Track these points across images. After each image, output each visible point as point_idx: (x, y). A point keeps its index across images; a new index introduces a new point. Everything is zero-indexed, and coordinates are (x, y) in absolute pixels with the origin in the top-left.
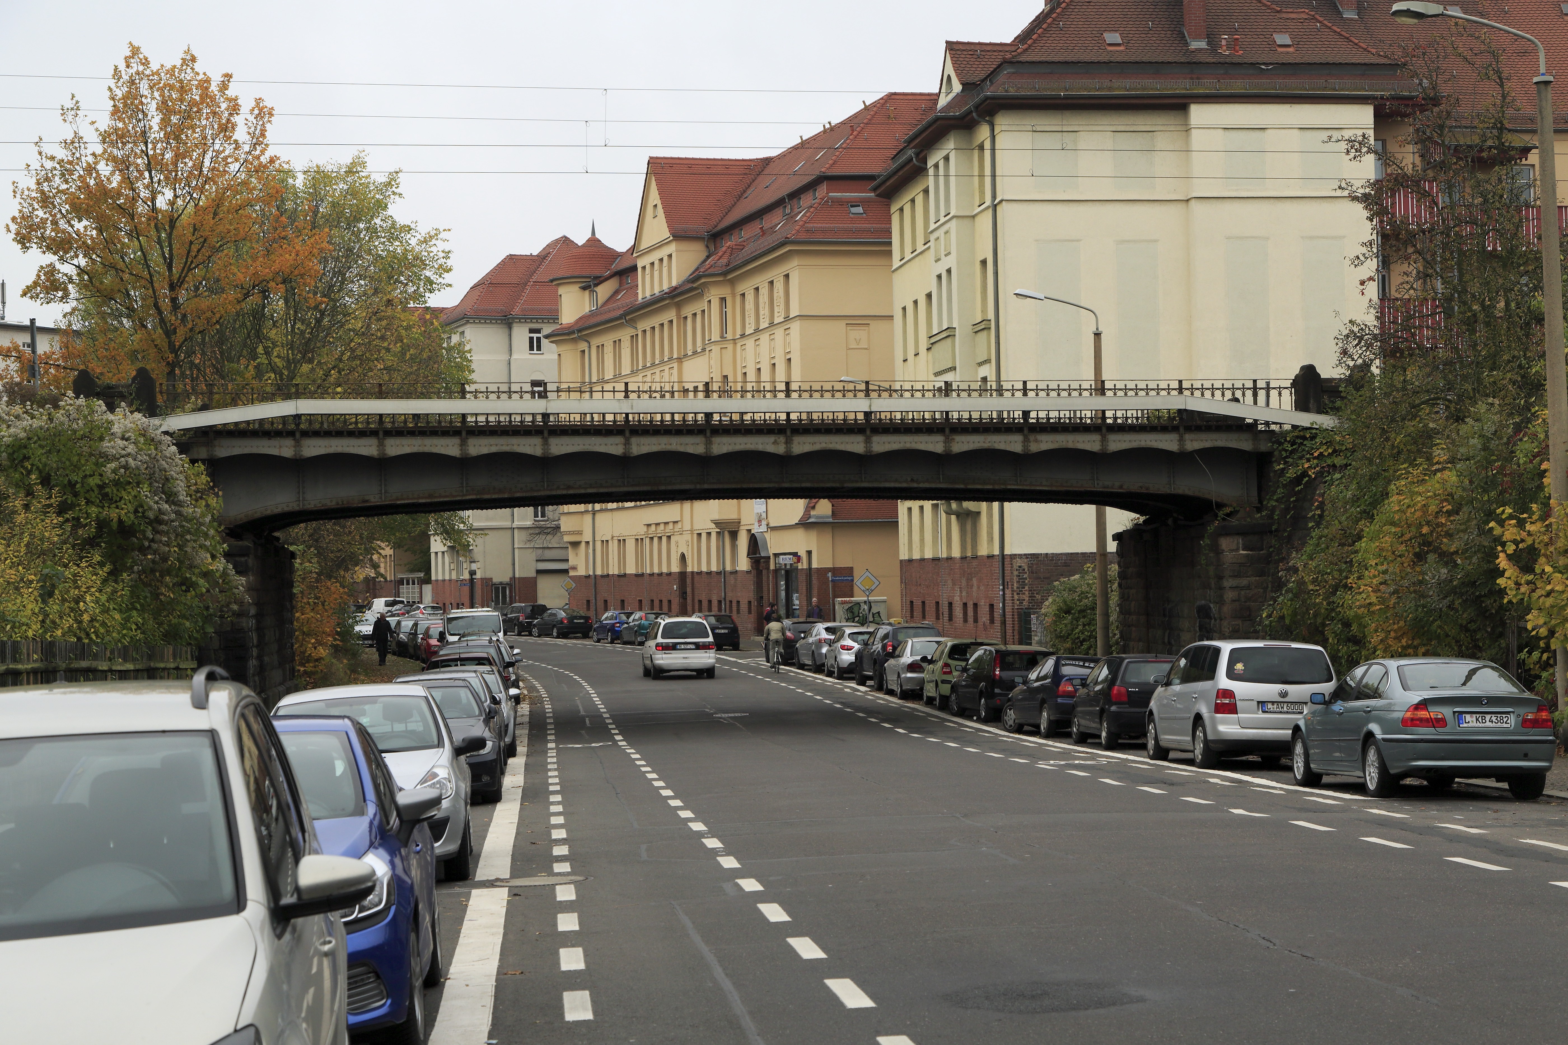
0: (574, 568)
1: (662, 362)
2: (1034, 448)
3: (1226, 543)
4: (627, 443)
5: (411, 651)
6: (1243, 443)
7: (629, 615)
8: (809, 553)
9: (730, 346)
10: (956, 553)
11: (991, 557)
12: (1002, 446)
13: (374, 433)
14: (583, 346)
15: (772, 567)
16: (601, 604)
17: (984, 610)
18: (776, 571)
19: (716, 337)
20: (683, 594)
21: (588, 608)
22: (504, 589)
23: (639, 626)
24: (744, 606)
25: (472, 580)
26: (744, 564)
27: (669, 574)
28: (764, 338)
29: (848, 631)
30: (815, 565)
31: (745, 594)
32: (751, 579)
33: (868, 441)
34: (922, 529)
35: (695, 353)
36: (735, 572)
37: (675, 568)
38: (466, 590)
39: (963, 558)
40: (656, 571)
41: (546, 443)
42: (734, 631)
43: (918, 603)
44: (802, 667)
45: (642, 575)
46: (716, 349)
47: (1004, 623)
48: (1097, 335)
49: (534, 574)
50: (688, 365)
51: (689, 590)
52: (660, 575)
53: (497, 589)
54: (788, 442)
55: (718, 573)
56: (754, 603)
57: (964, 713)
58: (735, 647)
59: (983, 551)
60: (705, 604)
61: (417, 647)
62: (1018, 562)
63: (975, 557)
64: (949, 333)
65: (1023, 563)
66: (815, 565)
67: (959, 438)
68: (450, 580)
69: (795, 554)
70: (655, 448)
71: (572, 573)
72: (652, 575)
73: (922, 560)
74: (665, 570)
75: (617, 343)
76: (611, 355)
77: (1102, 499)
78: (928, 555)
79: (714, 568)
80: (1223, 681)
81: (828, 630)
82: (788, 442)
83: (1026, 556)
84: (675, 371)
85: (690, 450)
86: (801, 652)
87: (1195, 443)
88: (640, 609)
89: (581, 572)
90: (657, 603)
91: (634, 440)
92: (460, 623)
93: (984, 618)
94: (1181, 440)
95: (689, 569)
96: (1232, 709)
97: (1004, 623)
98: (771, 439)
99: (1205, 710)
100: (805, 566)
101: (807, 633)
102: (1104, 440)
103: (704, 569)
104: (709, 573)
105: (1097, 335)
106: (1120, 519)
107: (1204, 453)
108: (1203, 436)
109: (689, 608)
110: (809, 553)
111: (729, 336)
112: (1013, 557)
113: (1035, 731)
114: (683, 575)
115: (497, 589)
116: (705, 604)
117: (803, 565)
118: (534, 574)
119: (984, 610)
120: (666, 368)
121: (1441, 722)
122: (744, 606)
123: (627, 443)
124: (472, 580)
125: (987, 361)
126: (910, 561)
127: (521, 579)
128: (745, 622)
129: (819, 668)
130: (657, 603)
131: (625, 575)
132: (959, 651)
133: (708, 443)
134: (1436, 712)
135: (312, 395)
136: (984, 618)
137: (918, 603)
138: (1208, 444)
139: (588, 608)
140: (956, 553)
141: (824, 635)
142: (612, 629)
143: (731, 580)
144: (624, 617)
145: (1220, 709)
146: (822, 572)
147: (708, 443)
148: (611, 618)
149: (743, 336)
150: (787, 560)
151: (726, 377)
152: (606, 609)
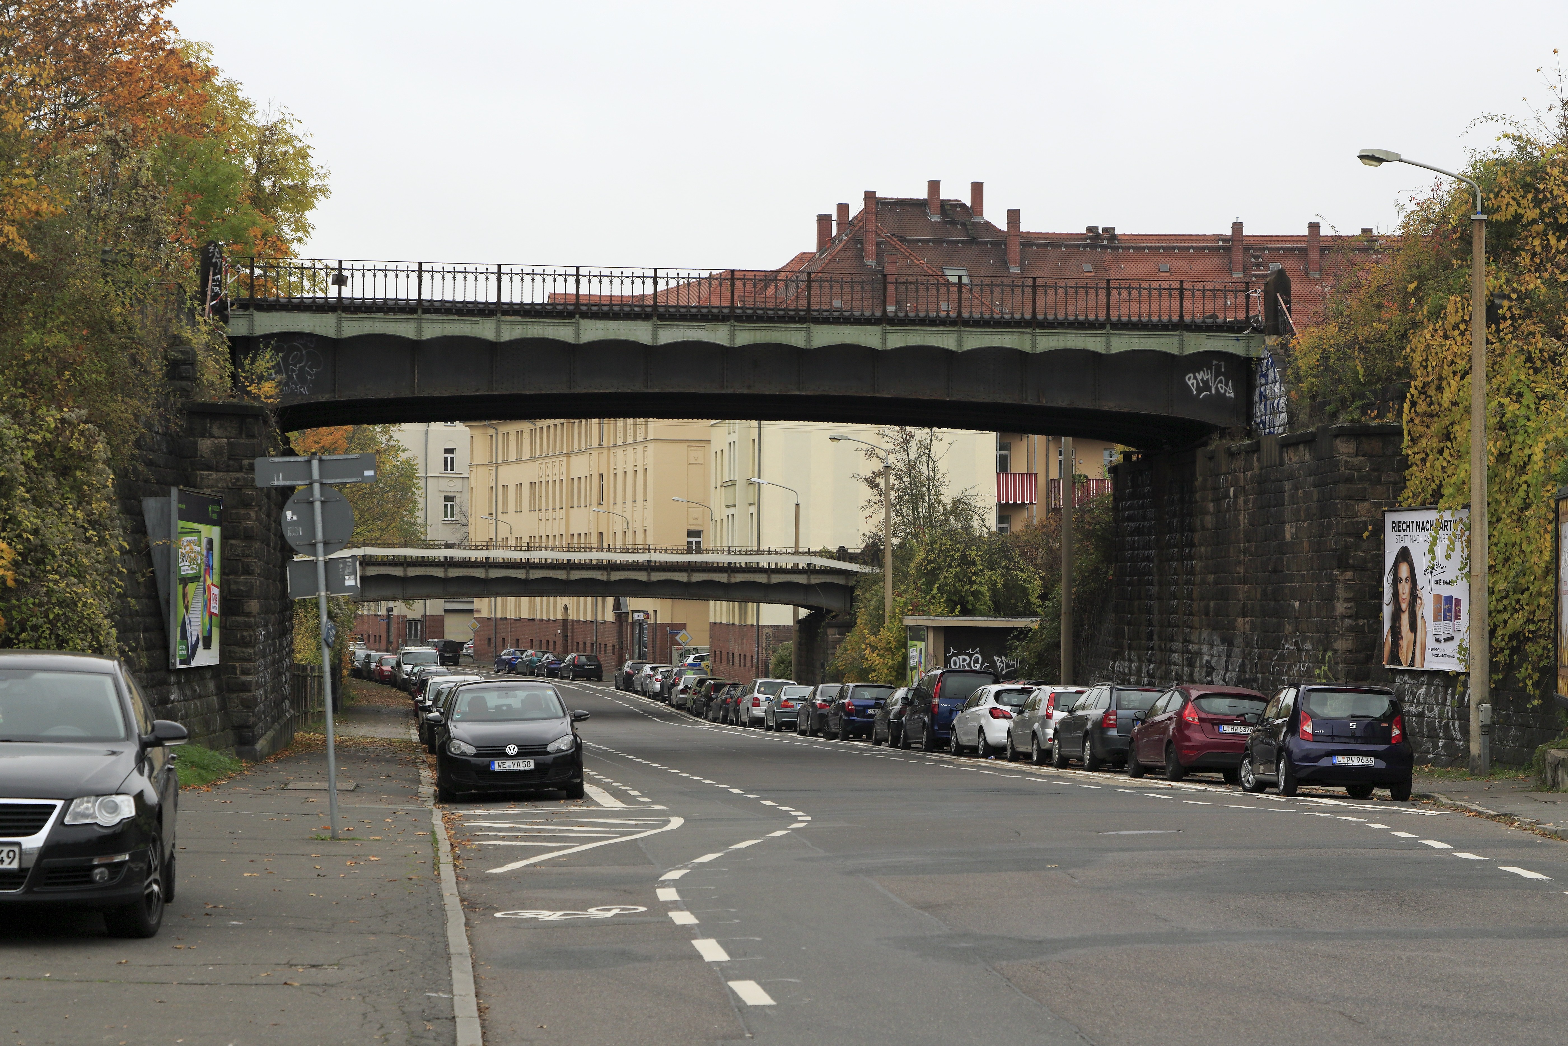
0: (479, 611)
1: (554, 455)
2: (733, 580)
3: (830, 631)
4: (528, 573)
5: (365, 674)
6: (840, 581)
7: (522, 652)
8: (655, 612)
9: (605, 452)
10: (737, 622)
11: (752, 626)
12: (717, 579)
13: (401, 565)
14: (492, 431)
15: (630, 620)
16: (500, 642)
17: (748, 659)
18: (633, 623)
19: (595, 444)
20: (565, 637)
21: (489, 644)
22: (416, 625)
23: (530, 661)
24: (610, 648)
25: (388, 616)
26: (610, 617)
27: (555, 621)
28: (630, 450)
29: (660, 670)
30: (658, 621)
31: (610, 640)
32: (614, 630)
33: (649, 575)
34: (721, 611)
35: (580, 451)
36: (604, 623)
37: (560, 616)
38: (384, 624)
39: (740, 625)
40: (545, 617)
41: (487, 572)
42: (599, 667)
43: (718, 652)
44: (636, 692)
45: (534, 620)
46: (595, 453)
47: (757, 667)
48: (797, 505)
49: (442, 613)
50: (575, 460)
51: (569, 634)
52: (548, 620)
53: (410, 624)
54: (609, 574)
55: (592, 622)
56: (617, 647)
57: (699, 715)
58: (600, 679)
59: (749, 623)
60: (581, 645)
61: (370, 671)
62: (766, 631)
63: (746, 625)
64: (732, 483)
65: (769, 631)
66: (658, 621)
67: (695, 575)
68: (369, 615)
69: (645, 612)
70: (541, 576)
71: (476, 615)
72: (541, 620)
73: (721, 624)
74: (552, 617)
75: (520, 433)
76: (514, 443)
77: (797, 605)
78: (724, 621)
79: (589, 618)
80: (756, 695)
81: (652, 668)
82: (609, 574)
83: (772, 626)
84: (564, 463)
85: (559, 577)
86: (636, 682)
87: (815, 580)
88: (532, 648)
89: (484, 614)
90: (544, 643)
91: (531, 571)
92: (411, 656)
93: (748, 665)
94: (809, 578)
95: (570, 618)
96: (758, 705)
97: (757, 667)
98: (600, 572)
99: (750, 705)
100: (652, 621)
101: (640, 670)
102: (769, 578)
103: (582, 619)
104: (585, 622)
105: (797, 505)
106: (803, 613)
107: (819, 584)
108: (820, 576)
109: (569, 648)
110: (655, 612)
111: (605, 444)
112: (764, 627)
113: (543, 675)
114: (565, 622)
115: (410, 624)
116: (581, 645)
117: (651, 621)
118: (442, 613)
119: (748, 659)
120: (558, 460)
121: (792, 706)
122: (610, 648)
123: (528, 573)
124: (388, 616)
125: (753, 504)
126: (715, 623)
127: (432, 617)
128: (607, 660)
129: (645, 694)
130: (544, 643)
131: (520, 619)
132: (701, 682)
133: (568, 574)
134: (790, 703)
135: (373, 546)
136: (748, 665)
137: (718, 652)
138: (822, 581)
139: (489, 644)
140: (737, 622)
141: (649, 672)
142: (509, 662)
143: (601, 627)
144: (518, 654)
145: (754, 705)
146: (664, 626)
147: (568, 574)
148: (509, 654)
149: (615, 445)
150: (639, 617)
151: (601, 475)
152: (504, 646)
